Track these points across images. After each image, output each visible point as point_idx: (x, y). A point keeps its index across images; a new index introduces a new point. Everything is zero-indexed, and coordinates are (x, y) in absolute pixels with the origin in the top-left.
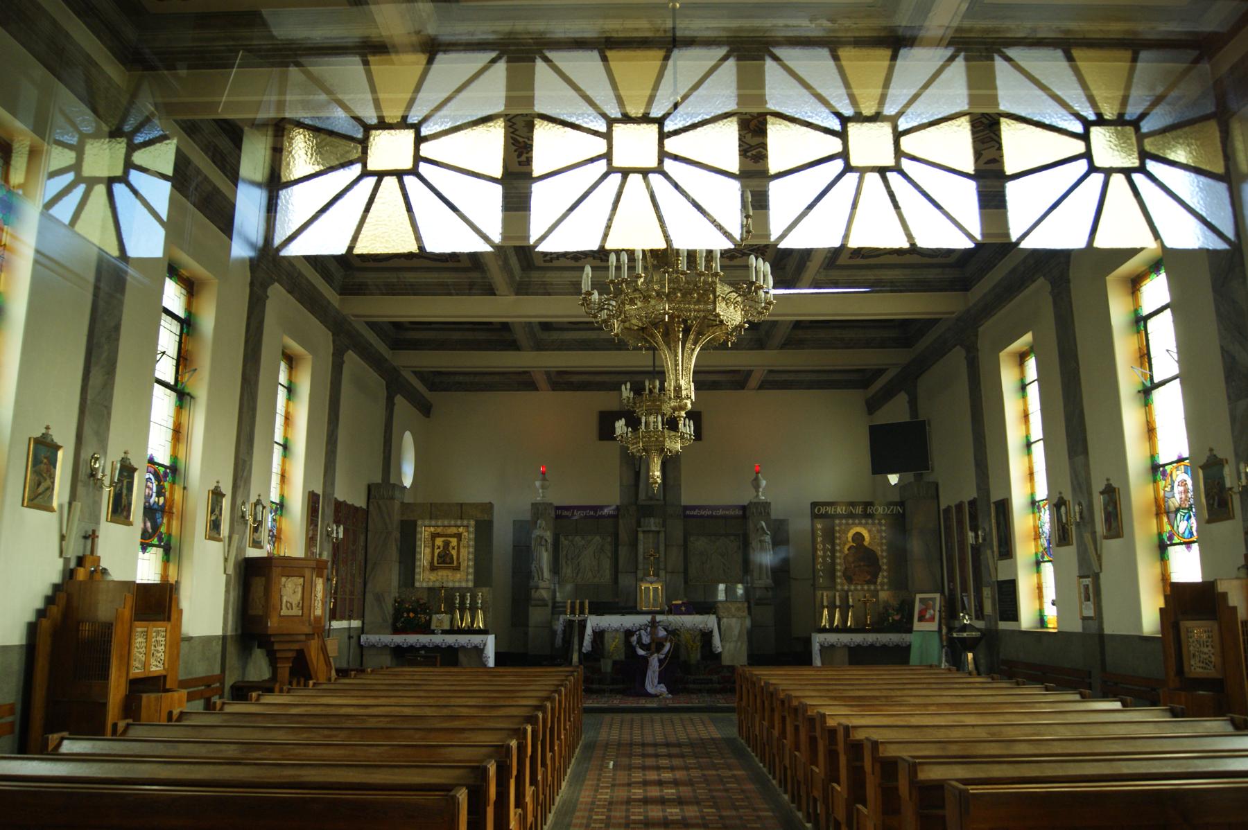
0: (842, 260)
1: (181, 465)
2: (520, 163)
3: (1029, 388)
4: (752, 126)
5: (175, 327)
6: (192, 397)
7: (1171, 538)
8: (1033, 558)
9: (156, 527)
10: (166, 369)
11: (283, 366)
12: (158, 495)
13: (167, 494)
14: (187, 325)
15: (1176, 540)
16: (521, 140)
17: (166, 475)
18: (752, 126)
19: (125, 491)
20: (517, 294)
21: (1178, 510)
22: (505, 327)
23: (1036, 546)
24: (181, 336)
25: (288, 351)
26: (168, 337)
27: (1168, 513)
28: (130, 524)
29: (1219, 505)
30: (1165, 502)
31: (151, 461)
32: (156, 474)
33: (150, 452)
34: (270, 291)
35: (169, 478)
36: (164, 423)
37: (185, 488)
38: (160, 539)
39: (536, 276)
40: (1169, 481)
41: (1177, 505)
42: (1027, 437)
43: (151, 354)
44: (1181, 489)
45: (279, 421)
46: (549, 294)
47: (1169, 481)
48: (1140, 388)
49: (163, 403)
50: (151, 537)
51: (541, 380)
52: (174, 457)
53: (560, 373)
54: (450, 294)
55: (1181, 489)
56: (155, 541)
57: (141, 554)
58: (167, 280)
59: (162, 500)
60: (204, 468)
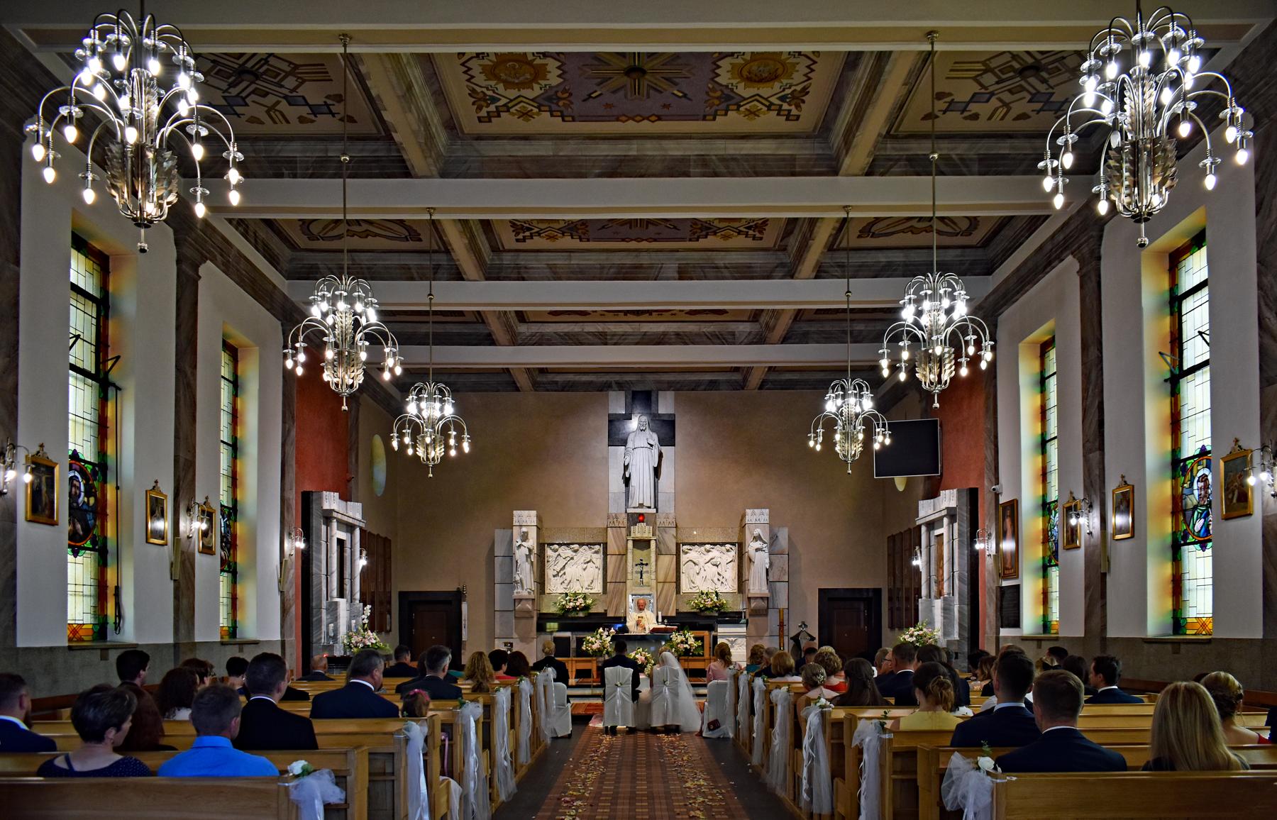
0: (852, 238)
1: (111, 462)
2: (480, 119)
3: (1187, 305)
4: (745, 73)
5: (92, 309)
6: (118, 389)
7: (1185, 537)
8: (1041, 563)
9: (87, 530)
10: (82, 354)
11: (224, 358)
12: (88, 494)
13: (98, 494)
14: (103, 305)
15: (1191, 539)
16: (479, 89)
17: (94, 473)
18: (745, 73)
19: (44, 488)
20: (487, 279)
21: (1195, 508)
22: (479, 317)
23: (1044, 551)
24: (98, 319)
25: (231, 341)
26: (80, 319)
27: (1184, 511)
28: (54, 524)
29: (1239, 500)
30: (1182, 499)
31: (75, 455)
32: (82, 472)
33: (71, 447)
34: (202, 270)
35: (99, 476)
36: (88, 417)
37: (117, 488)
38: (94, 542)
39: (507, 259)
40: (1188, 477)
41: (1195, 502)
42: (1043, 434)
43: (67, 340)
44: (1201, 484)
45: (225, 420)
46: (523, 279)
47: (1188, 477)
48: (1168, 376)
49: (80, 397)
50: (83, 539)
51: (523, 381)
52: (102, 452)
53: (543, 371)
54: (412, 279)
55: (1201, 484)
56: (88, 544)
57: (70, 558)
58: (74, 253)
59: (92, 500)
60: (139, 460)
